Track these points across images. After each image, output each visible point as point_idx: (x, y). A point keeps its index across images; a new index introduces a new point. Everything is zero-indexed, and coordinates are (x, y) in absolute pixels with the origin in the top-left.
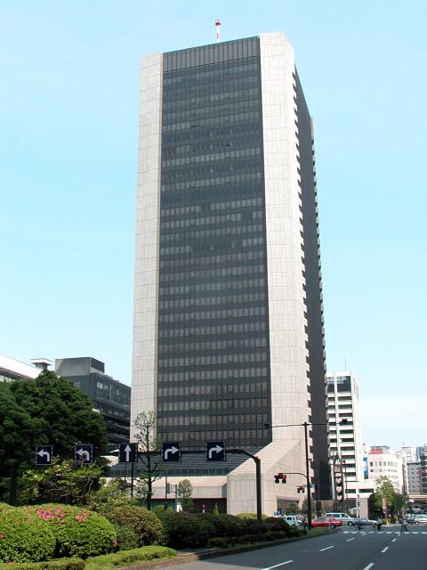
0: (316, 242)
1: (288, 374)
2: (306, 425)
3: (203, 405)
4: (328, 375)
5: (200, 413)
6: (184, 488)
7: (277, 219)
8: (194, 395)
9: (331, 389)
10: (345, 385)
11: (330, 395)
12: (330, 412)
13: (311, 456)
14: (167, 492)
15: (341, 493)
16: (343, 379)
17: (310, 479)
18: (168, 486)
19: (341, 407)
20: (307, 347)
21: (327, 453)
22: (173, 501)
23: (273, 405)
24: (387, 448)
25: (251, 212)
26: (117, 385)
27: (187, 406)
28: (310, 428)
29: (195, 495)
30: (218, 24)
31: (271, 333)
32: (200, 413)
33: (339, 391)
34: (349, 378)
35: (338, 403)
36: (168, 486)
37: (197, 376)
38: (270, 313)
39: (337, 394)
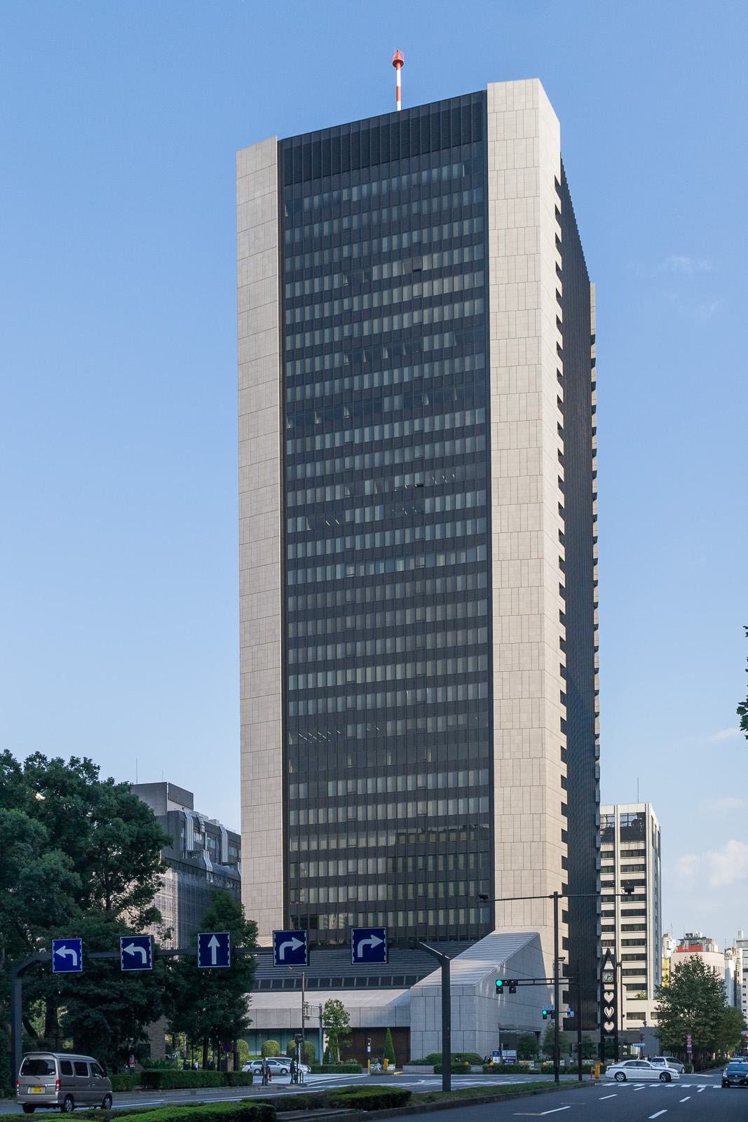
0: (589, 399)
1: (527, 810)
2: (555, 897)
3: (379, 865)
4: (604, 810)
5: (374, 879)
6: (334, 1013)
7: (513, 508)
8: (425, 789)
9: (609, 836)
10: (636, 828)
11: (605, 848)
12: (605, 921)
13: (564, 953)
14: (305, 1018)
15: (614, 1019)
16: (631, 819)
17: (561, 967)
18: (305, 1006)
19: (626, 928)
20: (563, 760)
21: (594, 906)
22: (314, 1032)
23: (498, 866)
24: (709, 941)
25: (381, 399)
26: (214, 830)
27: (340, 868)
28: (564, 904)
29: (353, 1023)
30: (396, 63)
31: (497, 734)
32: (374, 879)
33: (622, 840)
34: (642, 816)
35: (621, 861)
36: (305, 1006)
37: (362, 813)
38: (497, 695)
39: (621, 846)
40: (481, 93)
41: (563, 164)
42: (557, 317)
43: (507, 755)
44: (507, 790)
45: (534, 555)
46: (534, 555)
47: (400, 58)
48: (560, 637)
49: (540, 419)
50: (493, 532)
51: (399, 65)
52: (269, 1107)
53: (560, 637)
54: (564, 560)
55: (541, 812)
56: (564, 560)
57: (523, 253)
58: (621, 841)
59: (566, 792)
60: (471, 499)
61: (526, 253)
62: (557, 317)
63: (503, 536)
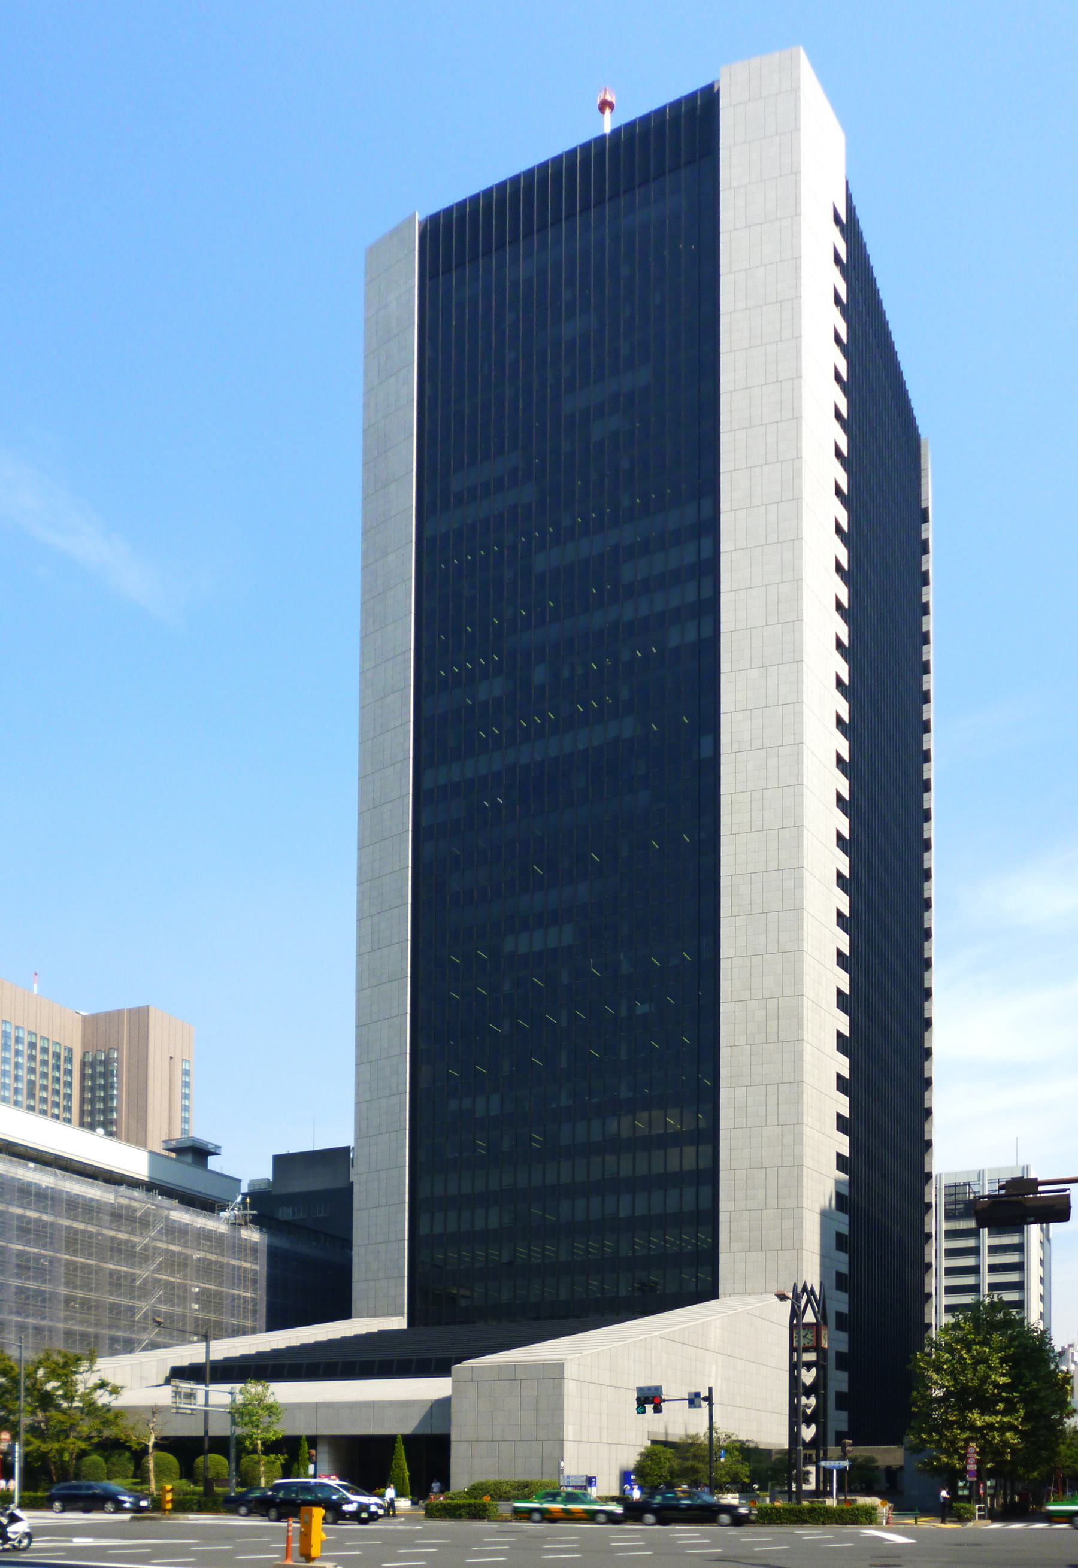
40: (711, 87)
41: (851, 190)
42: (835, 289)
43: (742, 1040)
44: (741, 1092)
45: (789, 739)
46: (789, 739)
47: (608, 98)
48: (838, 988)
49: (799, 538)
50: (722, 550)
51: (608, 111)
52: (505, 332)
53: (838, 988)
54: (847, 720)
55: (796, 1042)
56: (847, 720)
57: (775, 380)
58: (989, 1272)
59: (847, 1099)
60: (688, 1158)
61: (780, 1123)
62: (835, 289)
63: (735, 1247)
